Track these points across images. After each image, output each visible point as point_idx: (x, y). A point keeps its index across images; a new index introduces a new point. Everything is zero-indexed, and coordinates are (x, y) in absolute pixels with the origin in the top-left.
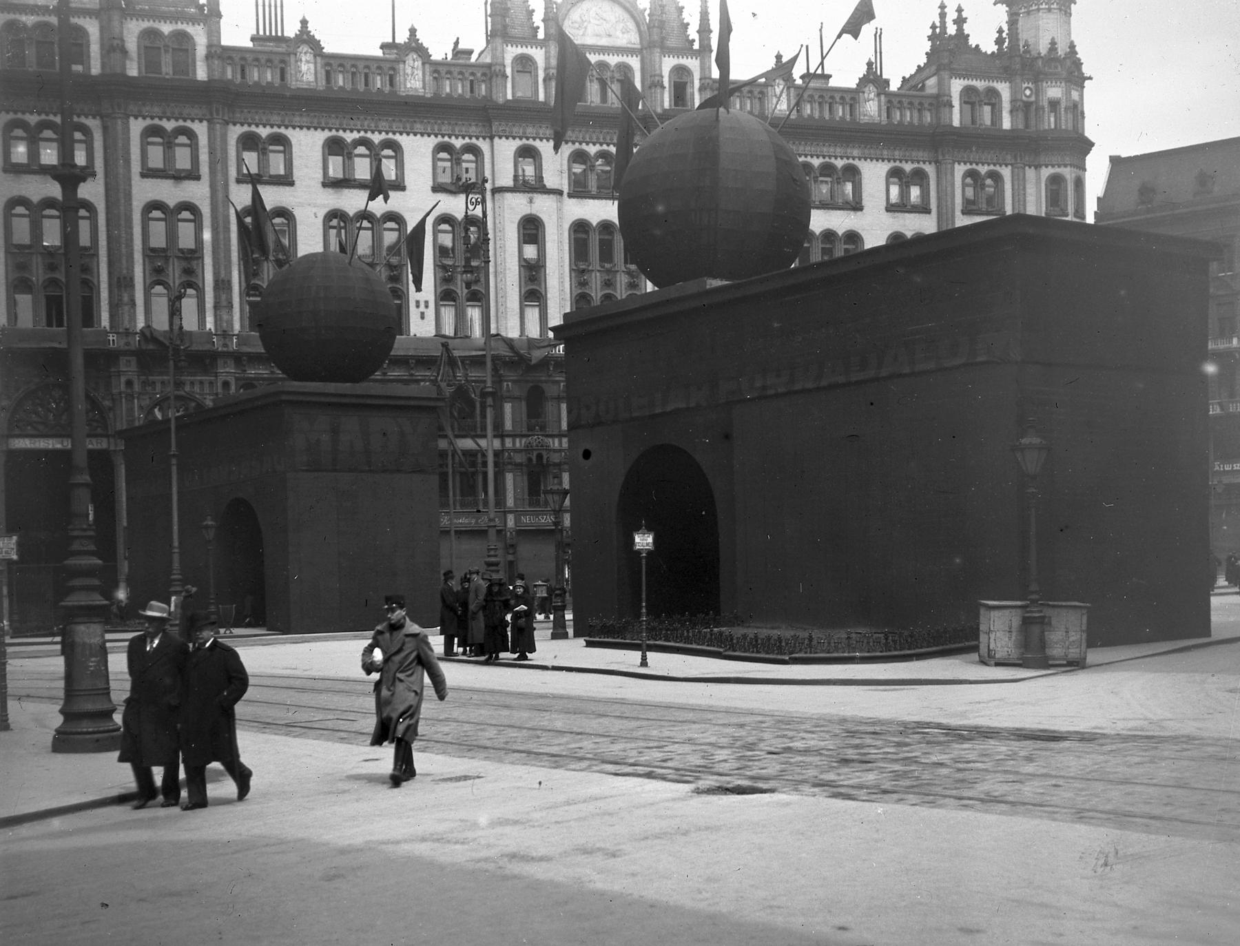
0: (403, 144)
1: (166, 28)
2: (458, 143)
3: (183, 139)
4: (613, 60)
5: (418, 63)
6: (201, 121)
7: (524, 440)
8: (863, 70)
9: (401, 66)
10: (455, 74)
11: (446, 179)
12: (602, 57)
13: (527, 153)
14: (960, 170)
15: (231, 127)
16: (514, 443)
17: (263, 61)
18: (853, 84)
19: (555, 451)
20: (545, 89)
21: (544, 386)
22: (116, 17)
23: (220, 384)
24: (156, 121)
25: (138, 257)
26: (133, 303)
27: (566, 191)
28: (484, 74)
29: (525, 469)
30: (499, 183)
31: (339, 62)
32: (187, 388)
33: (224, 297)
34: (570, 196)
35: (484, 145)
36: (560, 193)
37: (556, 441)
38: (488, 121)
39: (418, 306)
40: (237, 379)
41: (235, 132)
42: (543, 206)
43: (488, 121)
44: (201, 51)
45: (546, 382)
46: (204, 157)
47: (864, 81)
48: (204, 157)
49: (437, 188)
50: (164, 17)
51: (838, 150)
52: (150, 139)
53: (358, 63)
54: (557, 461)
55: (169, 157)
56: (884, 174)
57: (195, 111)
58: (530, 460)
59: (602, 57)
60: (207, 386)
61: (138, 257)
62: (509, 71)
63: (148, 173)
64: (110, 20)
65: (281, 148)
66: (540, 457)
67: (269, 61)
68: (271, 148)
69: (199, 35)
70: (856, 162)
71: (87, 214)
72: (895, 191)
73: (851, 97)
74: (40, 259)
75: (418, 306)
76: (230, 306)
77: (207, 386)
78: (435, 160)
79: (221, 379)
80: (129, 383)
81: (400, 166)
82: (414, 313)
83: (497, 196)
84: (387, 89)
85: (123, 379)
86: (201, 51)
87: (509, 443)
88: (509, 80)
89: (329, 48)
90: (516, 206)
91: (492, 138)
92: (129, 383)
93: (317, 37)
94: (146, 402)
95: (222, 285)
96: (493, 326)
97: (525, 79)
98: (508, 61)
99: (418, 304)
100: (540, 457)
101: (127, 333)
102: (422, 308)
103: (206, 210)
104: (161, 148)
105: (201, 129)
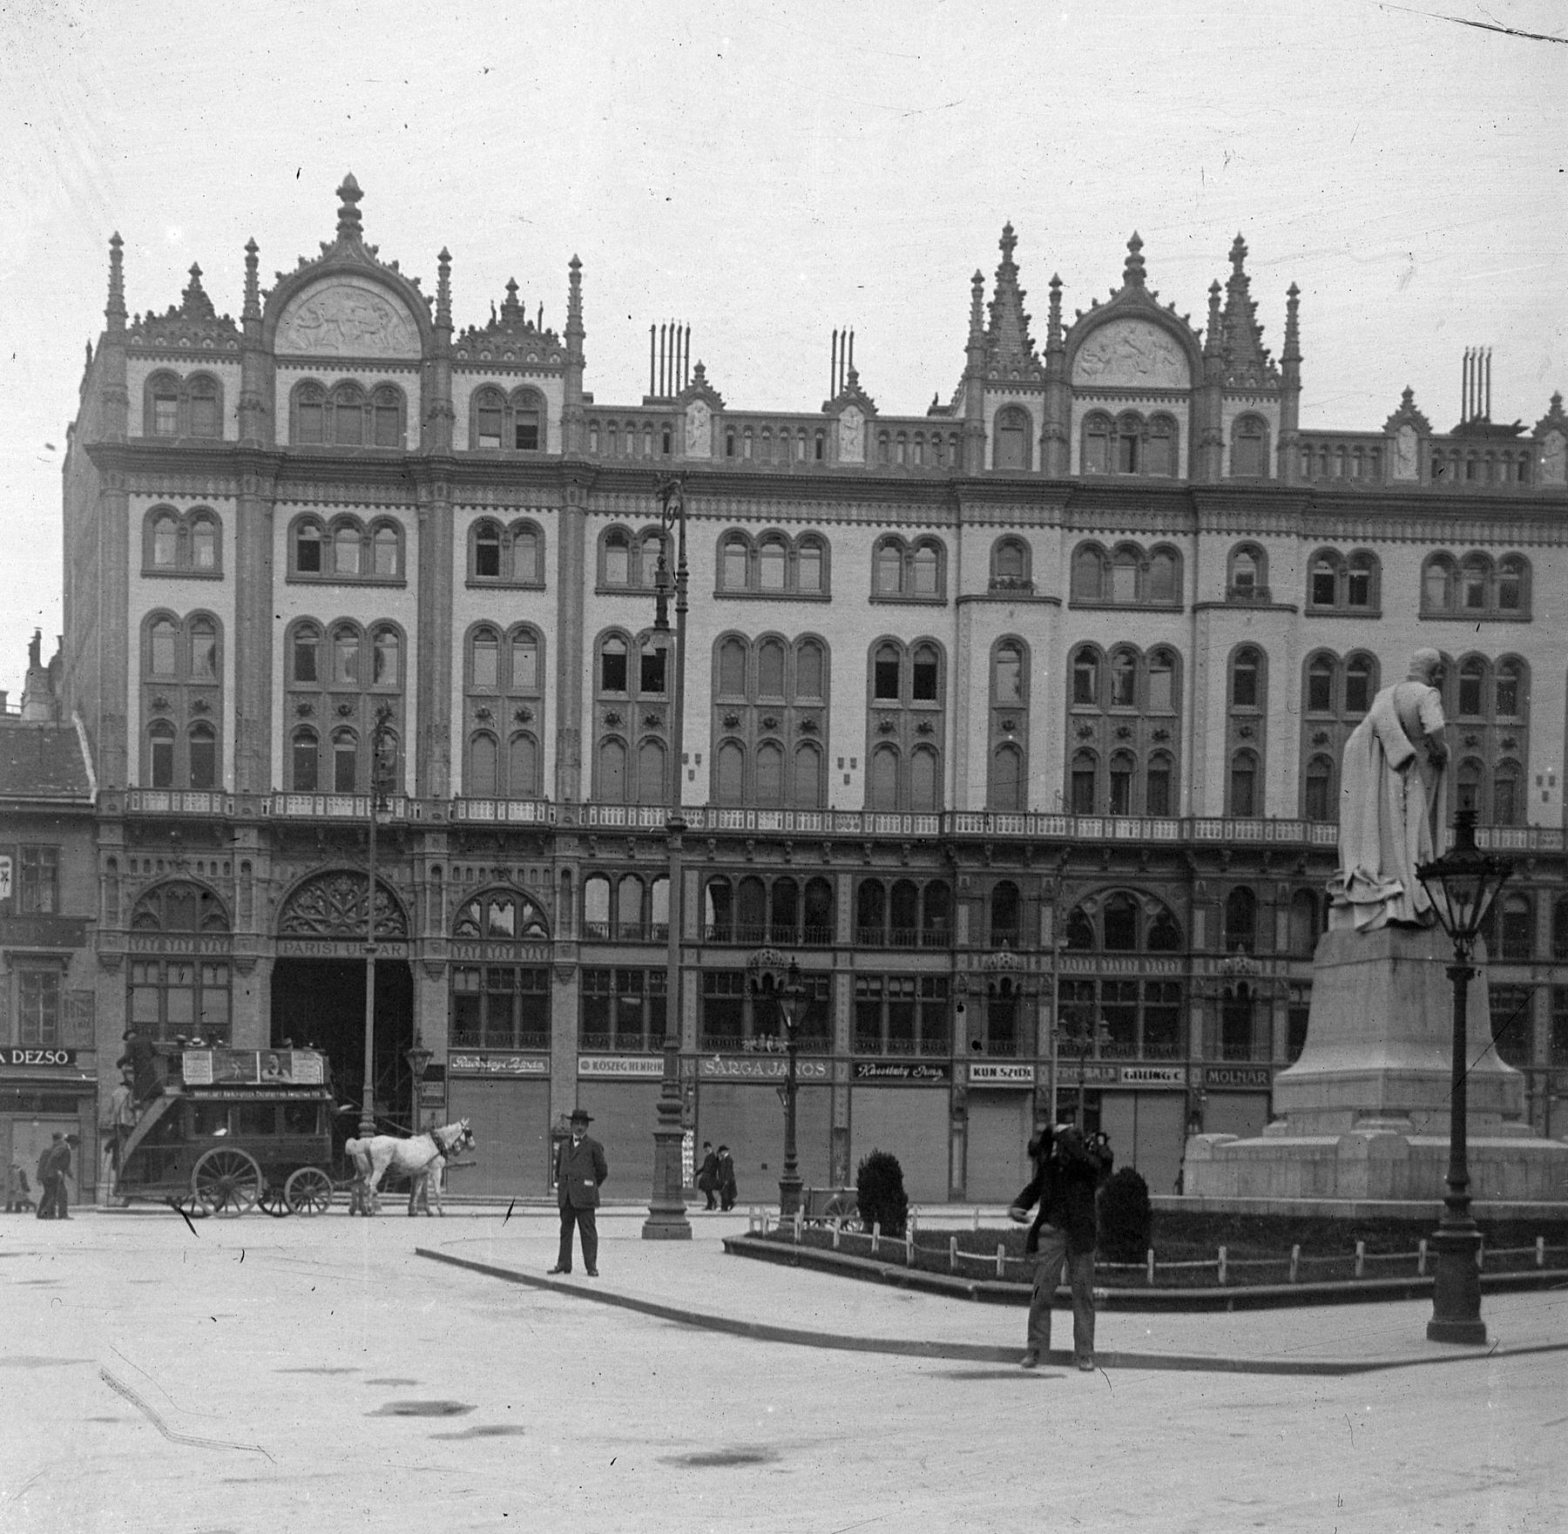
0: (1270, 550)
1: (508, 382)
2: (910, 534)
3: (926, 553)
4: (1147, 408)
5: (860, 419)
6: (227, 498)
7: (985, 958)
8: (1394, 404)
9: (834, 425)
10: (1350, 450)
11: (889, 588)
12: (1130, 404)
13: (1013, 545)
14: (464, 520)
15: (592, 517)
16: (1206, 968)
17: (640, 426)
18: (1376, 425)
19: (1029, 975)
20: (1043, 451)
21: (1018, 882)
22: (441, 371)
23: (558, 872)
24: (166, 500)
25: (457, 696)
26: (447, 761)
27: (1302, 606)
28: (953, 435)
29: (985, 1001)
30: (1203, 598)
31: (1338, 443)
32: (515, 877)
33: (569, 751)
34: (1072, 607)
35: (946, 535)
36: (1056, 602)
37: (1033, 959)
38: (1194, 511)
39: (841, 766)
40: (582, 867)
41: (596, 526)
42: (1027, 621)
43: (1194, 511)
44: (554, 413)
45: (1020, 875)
46: (552, 560)
47: (1395, 422)
48: (552, 560)
49: (877, 599)
50: (507, 368)
51: (1017, 513)
52: (731, 547)
53: (755, 424)
54: (1032, 990)
55: (752, 573)
56: (1420, 561)
57: (544, 498)
58: (1228, 991)
59: (1130, 404)
60: (541, 875)
61: (457, 696)
62: (989, 430)
63: (604, 590)
64: (435, 374)
65: (817, 552)
66: (1243, 987)
67: (649, 424)
68: (803, 551)
69: (552, 389)
70: (1525, 550)
71: (395, 640)
72: (1437, 590)
73: (815, 429)
74: (637, 710)
75: (841, 766)
76: (578, 764)
77: (541, 875)
78: (875, 560)
79: (561, 865)
80: (437, 870)
81: (825, 568)
82: (1534, 793)
83: (1201, 615)
84: (813, 459)
85: (429, 864)
86: (554, 413)
87: (962, 962)
88: (990, 441)
89: (884, 411)
90: (994, 621)
91: (1196, 533)
92: (437, 870)
93: (1425, 414)
94: (458, 897)
95: (568, 736)
96: (948, 795)
97: (1013, 441)
98: (1227, 422)
99: (1540, 781)
100: (1243, 987)
101: (436, 801)
102: (847, 769)
103: (551, 636)
104: (781, 561)
105: (549, 522)
